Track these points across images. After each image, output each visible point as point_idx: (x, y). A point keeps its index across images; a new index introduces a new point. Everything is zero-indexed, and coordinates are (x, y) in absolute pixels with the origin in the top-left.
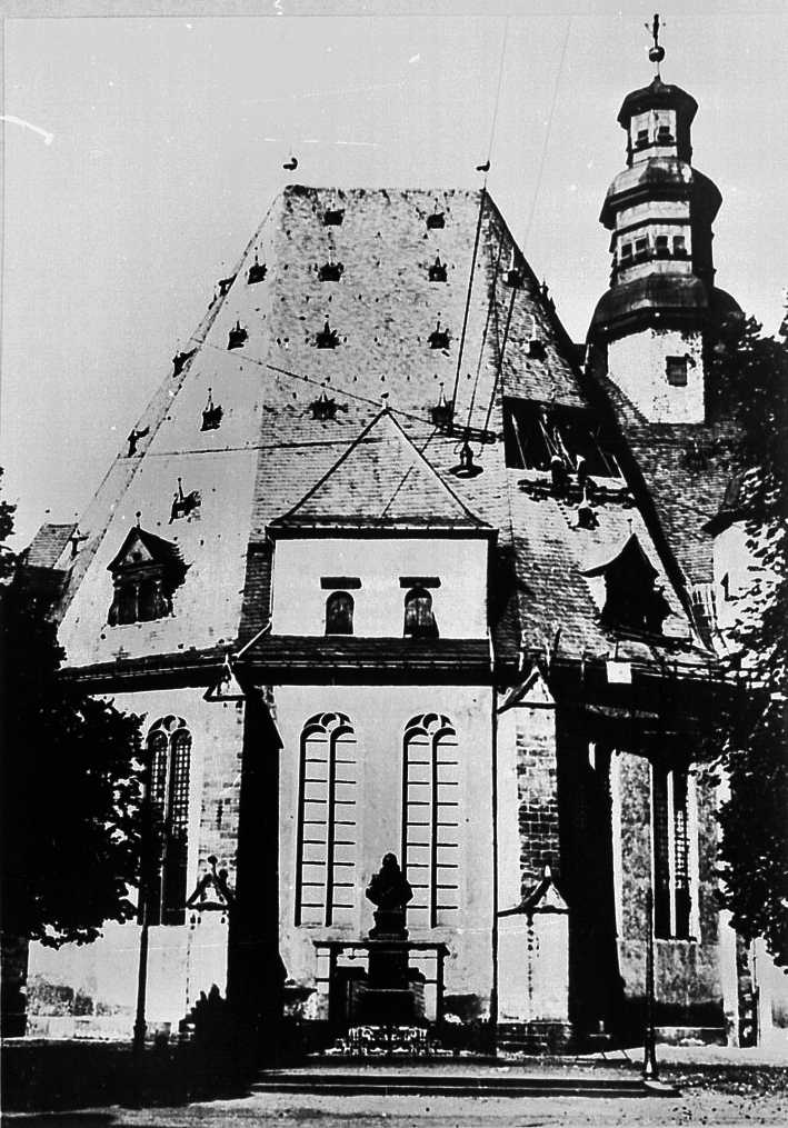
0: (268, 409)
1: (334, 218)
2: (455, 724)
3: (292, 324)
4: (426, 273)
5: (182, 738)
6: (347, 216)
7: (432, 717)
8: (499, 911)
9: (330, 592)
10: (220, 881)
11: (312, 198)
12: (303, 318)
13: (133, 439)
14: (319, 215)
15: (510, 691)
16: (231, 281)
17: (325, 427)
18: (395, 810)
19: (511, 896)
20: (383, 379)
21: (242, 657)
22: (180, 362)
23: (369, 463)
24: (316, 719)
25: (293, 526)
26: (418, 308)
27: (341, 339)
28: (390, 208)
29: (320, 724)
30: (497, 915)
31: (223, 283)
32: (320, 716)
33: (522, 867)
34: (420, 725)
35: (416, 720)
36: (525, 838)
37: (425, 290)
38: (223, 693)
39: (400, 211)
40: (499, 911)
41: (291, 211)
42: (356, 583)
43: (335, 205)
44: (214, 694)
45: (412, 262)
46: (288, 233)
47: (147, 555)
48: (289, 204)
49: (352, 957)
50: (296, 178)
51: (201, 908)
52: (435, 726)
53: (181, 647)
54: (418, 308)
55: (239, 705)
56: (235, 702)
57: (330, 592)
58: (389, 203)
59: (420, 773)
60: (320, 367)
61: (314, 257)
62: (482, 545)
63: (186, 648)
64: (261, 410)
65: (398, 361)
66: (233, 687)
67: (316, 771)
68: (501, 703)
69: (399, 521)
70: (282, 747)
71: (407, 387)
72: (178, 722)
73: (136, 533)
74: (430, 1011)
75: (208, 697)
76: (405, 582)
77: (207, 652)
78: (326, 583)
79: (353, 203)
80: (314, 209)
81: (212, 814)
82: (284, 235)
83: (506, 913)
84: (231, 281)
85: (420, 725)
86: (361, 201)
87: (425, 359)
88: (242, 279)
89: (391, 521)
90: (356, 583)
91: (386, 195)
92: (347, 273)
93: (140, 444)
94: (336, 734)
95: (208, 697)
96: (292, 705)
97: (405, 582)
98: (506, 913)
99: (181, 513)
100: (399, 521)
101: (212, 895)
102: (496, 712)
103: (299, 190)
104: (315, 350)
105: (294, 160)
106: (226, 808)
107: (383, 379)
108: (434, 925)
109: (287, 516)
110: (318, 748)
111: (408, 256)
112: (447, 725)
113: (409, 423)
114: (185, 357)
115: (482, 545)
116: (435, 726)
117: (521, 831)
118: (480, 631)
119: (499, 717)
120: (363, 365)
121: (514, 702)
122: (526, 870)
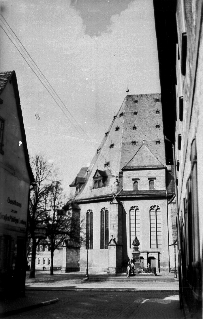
0: (123, 144)
1: (136, 102)
2: (160, 207)
3: (128, 125)
4: (155, 112)
5: (107, 211)
6: (138, 101)
7: (155, 206)
8: (169, 245)
9: (134, 181)
10: (114, 240)
11: (132, 97)
12: (130, 124)
13: (98, 150)
14: (133, 101)
15: (170, 200)
16: (116, 116)
17: (134, 146)
18: (95, 233)
19: (171, 242)
20: (146, 136)
21: (117, 195)
22: (107, 134)
23: (141, 155)
24: (132, 207)
25: (125, 169)
26: (153, 120)
27: (137, 128)
28: (148, 98)
29: (133, 208)
30: (169, 246)
31: (114, 117)
32: (133, 206)
33: (173, 236)
34: (153, 208)
35: (152, 207)
36: (173, 230)
37: (155, 115)
38: (113, 203)
39: (150, 99)
40: (169, 245)
41: (128, 101)
42: (139, 179)
43: (136, 99)
44: (112, 203)
45: (152, 110)
46: (127, 106)
47: (99, 175)
48: (127, 99)
49: (152, 255)
50: (130, 93)
51: (110, 245)
52: (156, 208)
53: (106, 193)
54: (153, 120)
55: (117, 205)
56: (116, 204)
57: (134, 181)
58: (148, 97)
59: (153, 217)
60: (133, 134)
61: (132, 110)
62: (164, 170)
63: (107, 194)
64: (122, 144)
65: (149, 131)
66: (115, 201)
67: (133, 217)
68: (168, 202)
69: (147, 166)
70: (126, 213)
71: (150, 137)
72: (106, 208)
73: (97, 171)
74: (70, 258)
75: (111, 204)
76: (149, 179)
77: (110, 195)
78: (133, 180)
79: (140, 98)
80: (132, 100)
81: (112, 227)
82: (126, 106)
83: (170, 245)
84: (116, 116)
85: (153, 208)
86: (141, 97)
87: (154, 131)
88: (118, 116)
89: (145, 166)
90: (139, 179)
91: (147, 96)
92: (138, 113)
93: (99, 151)
94: (136, 210)
95: (111, 204)
96: (127, 205)
97: (149, 179)
98: (170, 245)
99: (106, 166)
100: (147, 166)
101: (112, 243)
102: (168, 204)
103: (129, 96)
104: (132, 130)
105: (128, 90)
106: (115, 226)
107: (146, 136)
108: (157, 248)
109: (125, 167)
110: (133, 212)
111: (151, 109)
112: (158, 208)
113: (151, 145)
114: (107, 133)
115: (164, 170)
116: (156, 208)
117: (172, 229)
118: (165, 189)
119: (168, 205)
120: (141, 133)
121: (171, 203)
122: (174, 237)
